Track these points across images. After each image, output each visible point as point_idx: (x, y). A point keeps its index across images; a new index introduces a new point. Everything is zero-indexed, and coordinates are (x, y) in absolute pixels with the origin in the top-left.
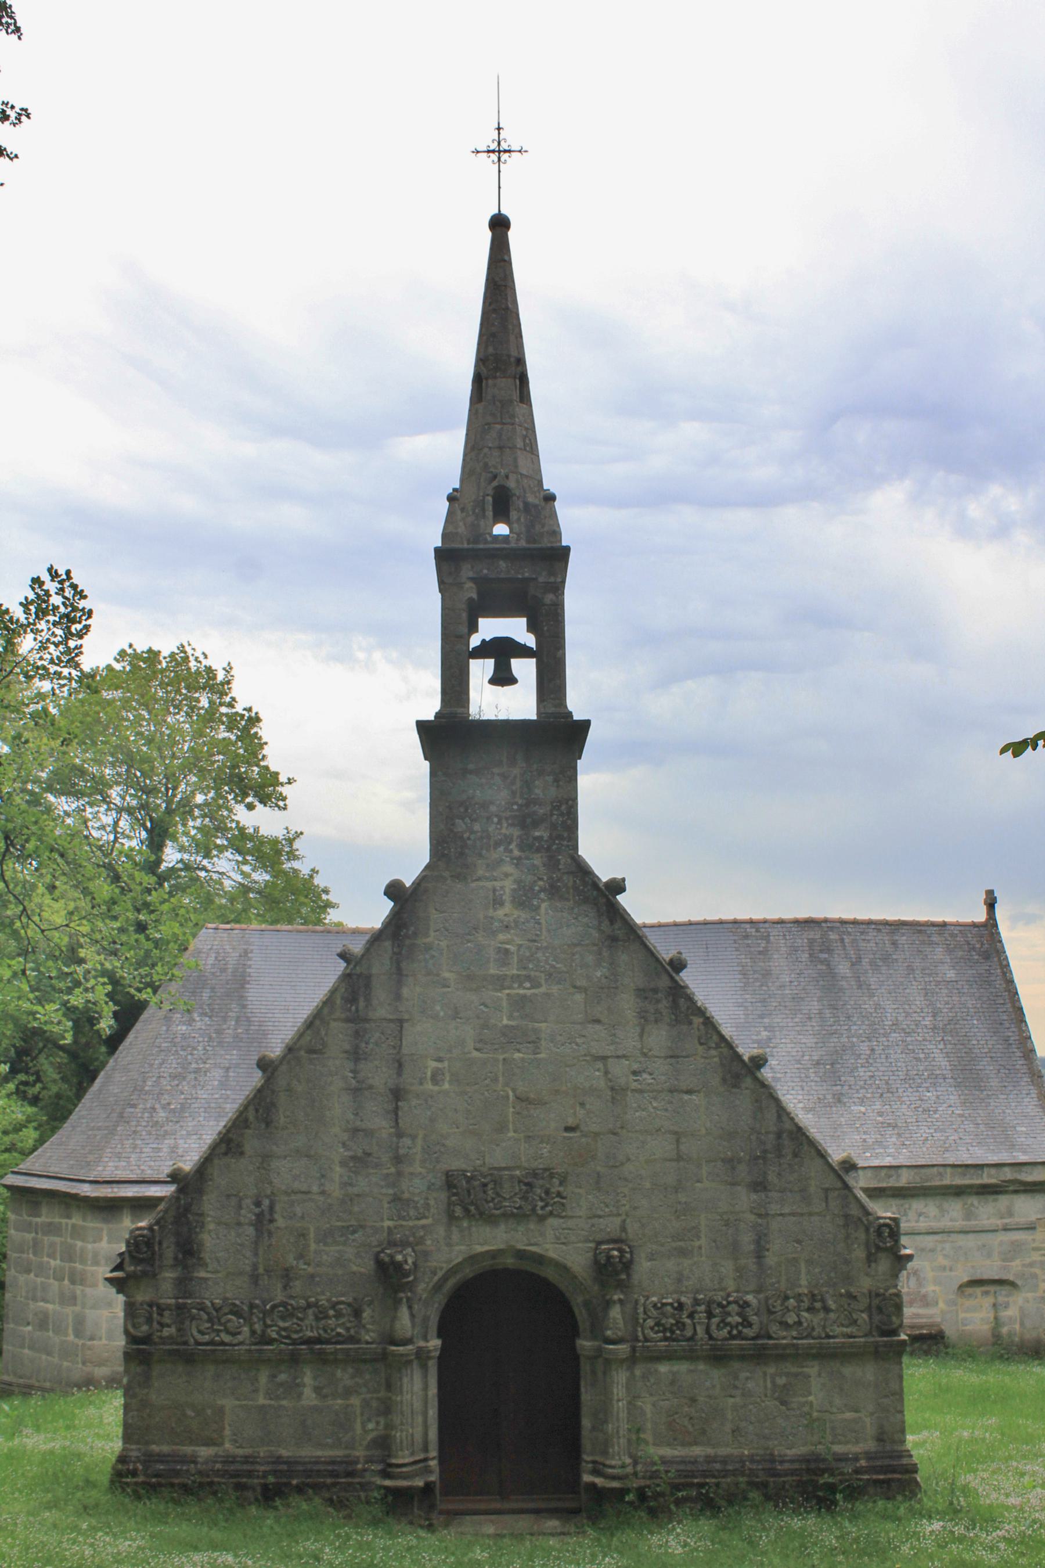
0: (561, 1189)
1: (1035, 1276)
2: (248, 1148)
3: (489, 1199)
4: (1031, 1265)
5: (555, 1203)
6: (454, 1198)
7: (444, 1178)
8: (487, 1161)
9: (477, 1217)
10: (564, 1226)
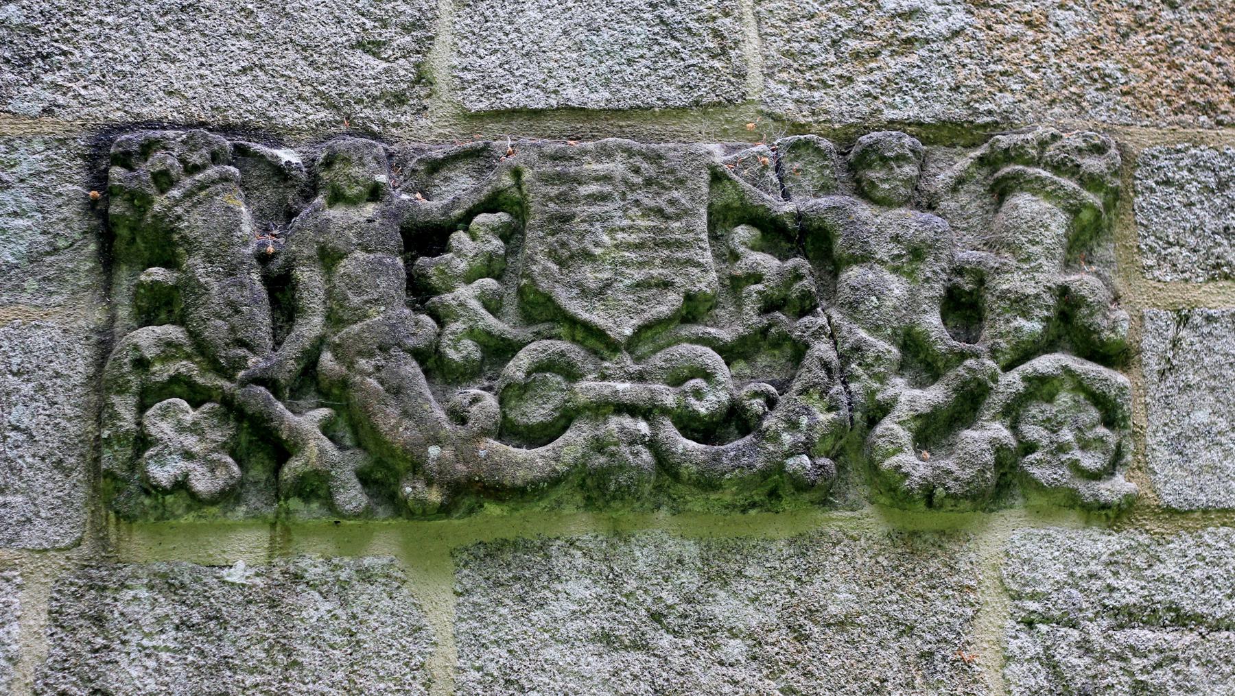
0: (1084, 281)
3: (461, 351)
5: (1040, 387)
6: (147, 338)
7: (74, 187)
8: (442, 60)
9: (352, 496)
10: (1129, 590)
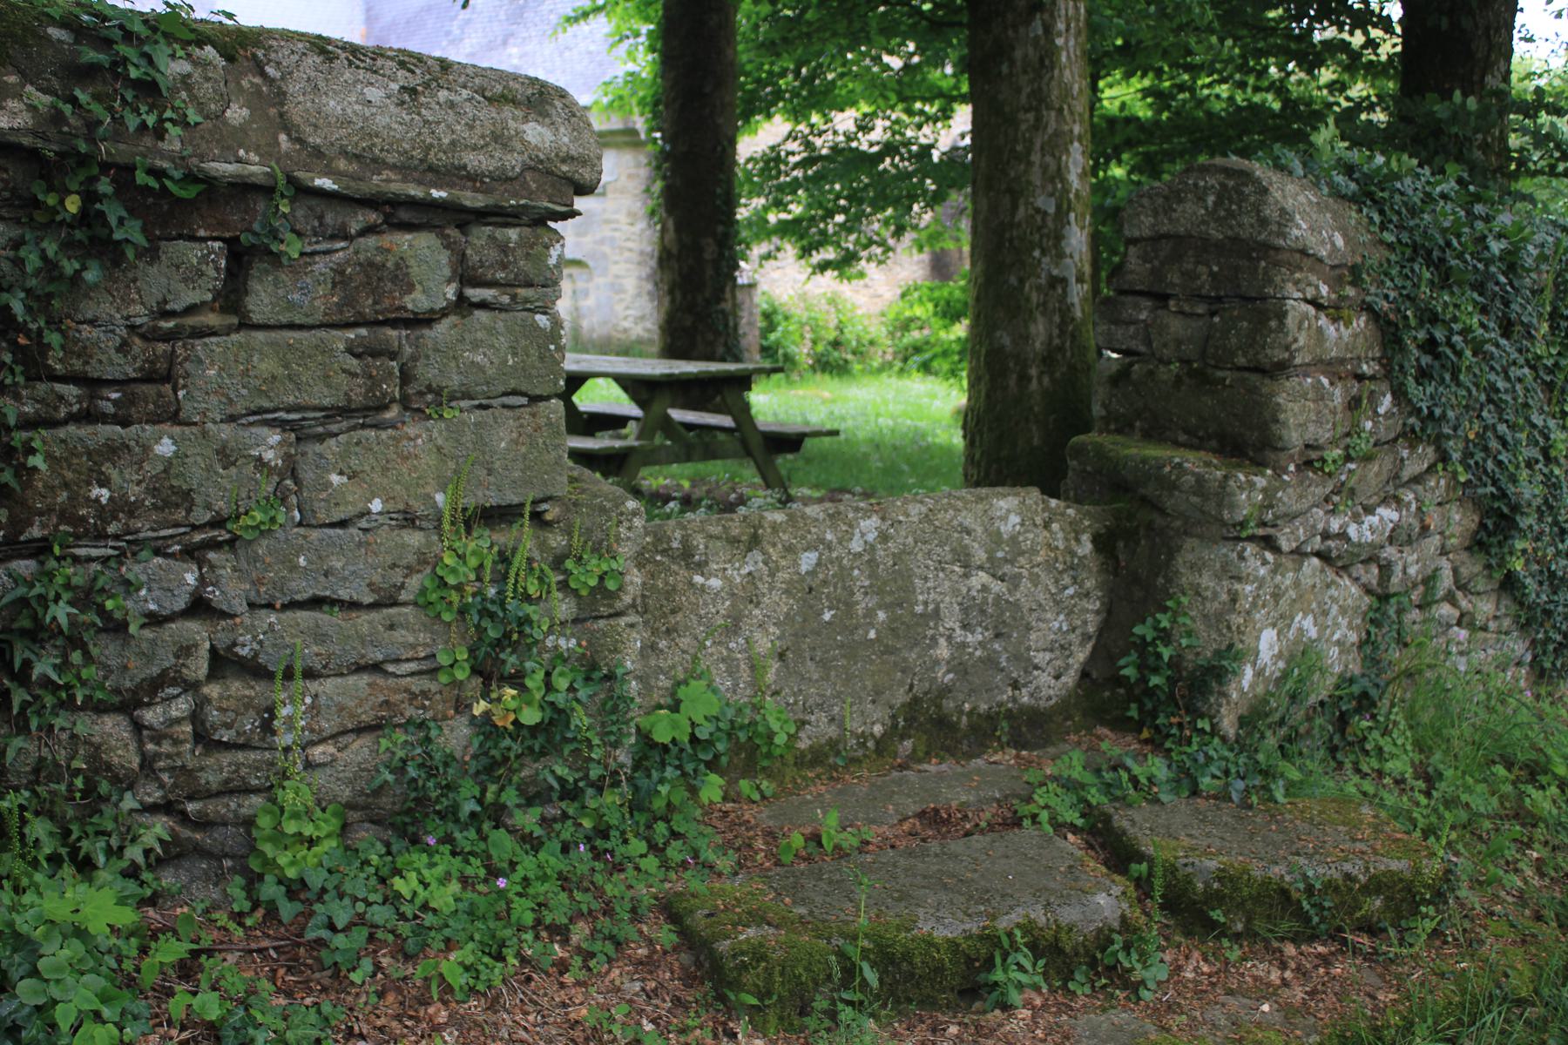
1: (604, 256)
2: (542, 855)
4: (602, 242)
